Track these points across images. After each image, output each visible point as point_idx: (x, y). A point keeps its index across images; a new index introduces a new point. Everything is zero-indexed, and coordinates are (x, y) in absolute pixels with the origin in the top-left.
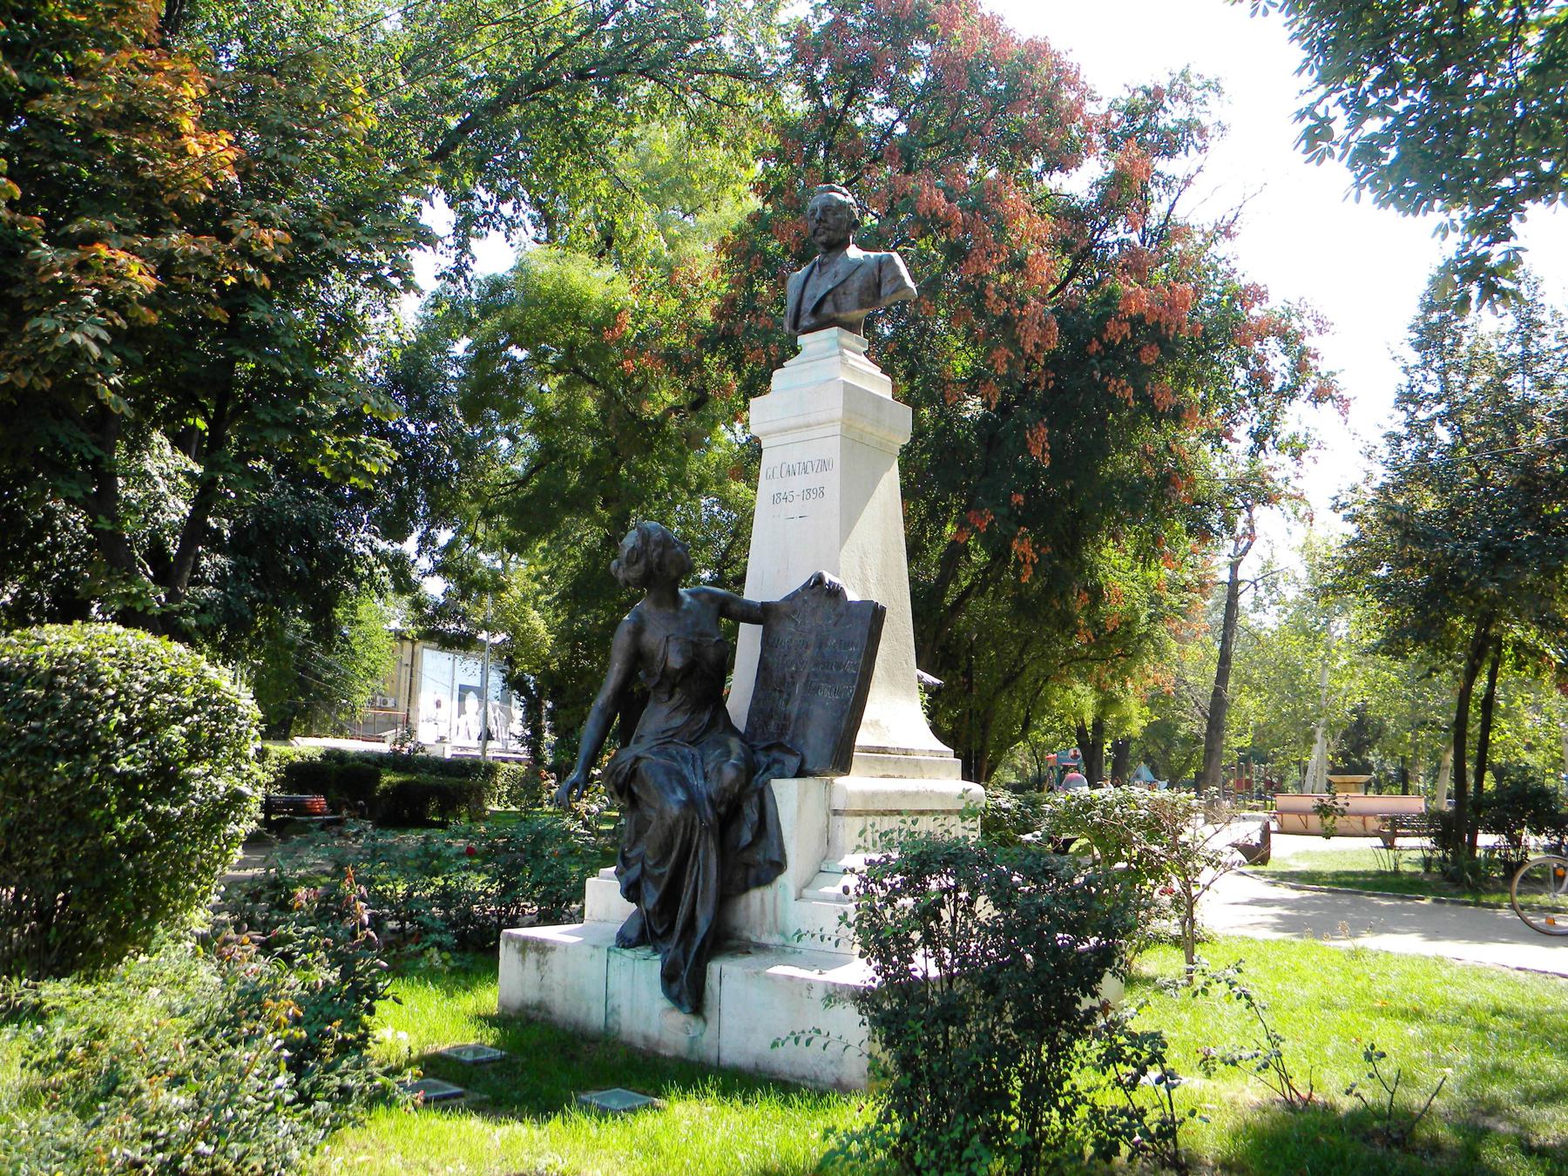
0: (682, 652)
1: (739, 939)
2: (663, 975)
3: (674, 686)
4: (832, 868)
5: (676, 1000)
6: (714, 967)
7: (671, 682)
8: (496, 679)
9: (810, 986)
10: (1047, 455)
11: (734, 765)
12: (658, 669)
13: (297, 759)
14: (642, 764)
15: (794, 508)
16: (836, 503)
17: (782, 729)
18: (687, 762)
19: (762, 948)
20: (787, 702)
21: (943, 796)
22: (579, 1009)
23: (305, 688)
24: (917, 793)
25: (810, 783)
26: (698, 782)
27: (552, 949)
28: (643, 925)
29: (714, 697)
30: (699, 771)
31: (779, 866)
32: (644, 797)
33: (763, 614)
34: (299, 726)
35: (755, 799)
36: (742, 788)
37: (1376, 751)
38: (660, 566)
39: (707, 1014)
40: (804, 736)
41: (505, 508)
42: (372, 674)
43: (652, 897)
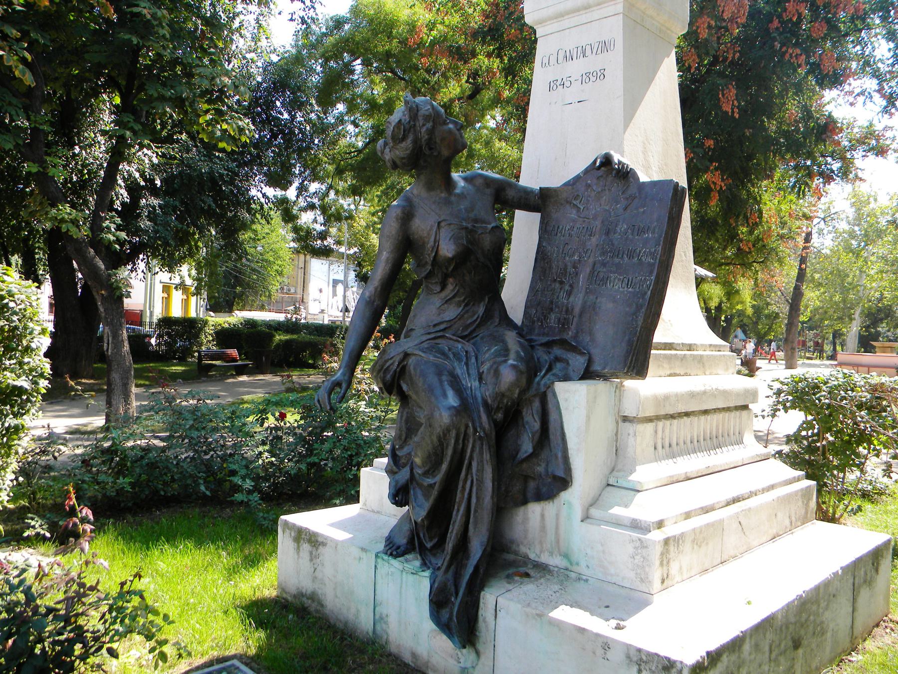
0: (455, 238)
1: (516, 553)
2: (431, 601)
3: (446, 277)
4: (621, 482)
5: (445, 627)
6: (489, 597)
7: (441, 272)
8: (352, 275)
9: (606, 645)
10: (736, 110)
11: (514, 367)
12: (429, 259)
13: (226, 326)
14: (411, 361)
15: (572, 93)
16: (620, 83)
17: (564, 324)
18: (459, 360)
19: (543, 568)
20: (569, 294)
21: (725, 393)
22: (348, 609)
23: (238, 281)
24: (705, 392)
25: (599, 386)
26: (471, 383)
27: (324, 544)
28: (412, 531)
29: (494, 283)
30: (474, 372)
31: (563, 482)
32: (414, 397)
33: (541, 201)
34: (238, 304)
35: (537, 404)
36: (523, 392)
37: (884, 325)
38: (430, 142)
39: (480, 646)
40: (591, 333)
41: (353, 168)
42: (280, 274)
43: (420, 509)
